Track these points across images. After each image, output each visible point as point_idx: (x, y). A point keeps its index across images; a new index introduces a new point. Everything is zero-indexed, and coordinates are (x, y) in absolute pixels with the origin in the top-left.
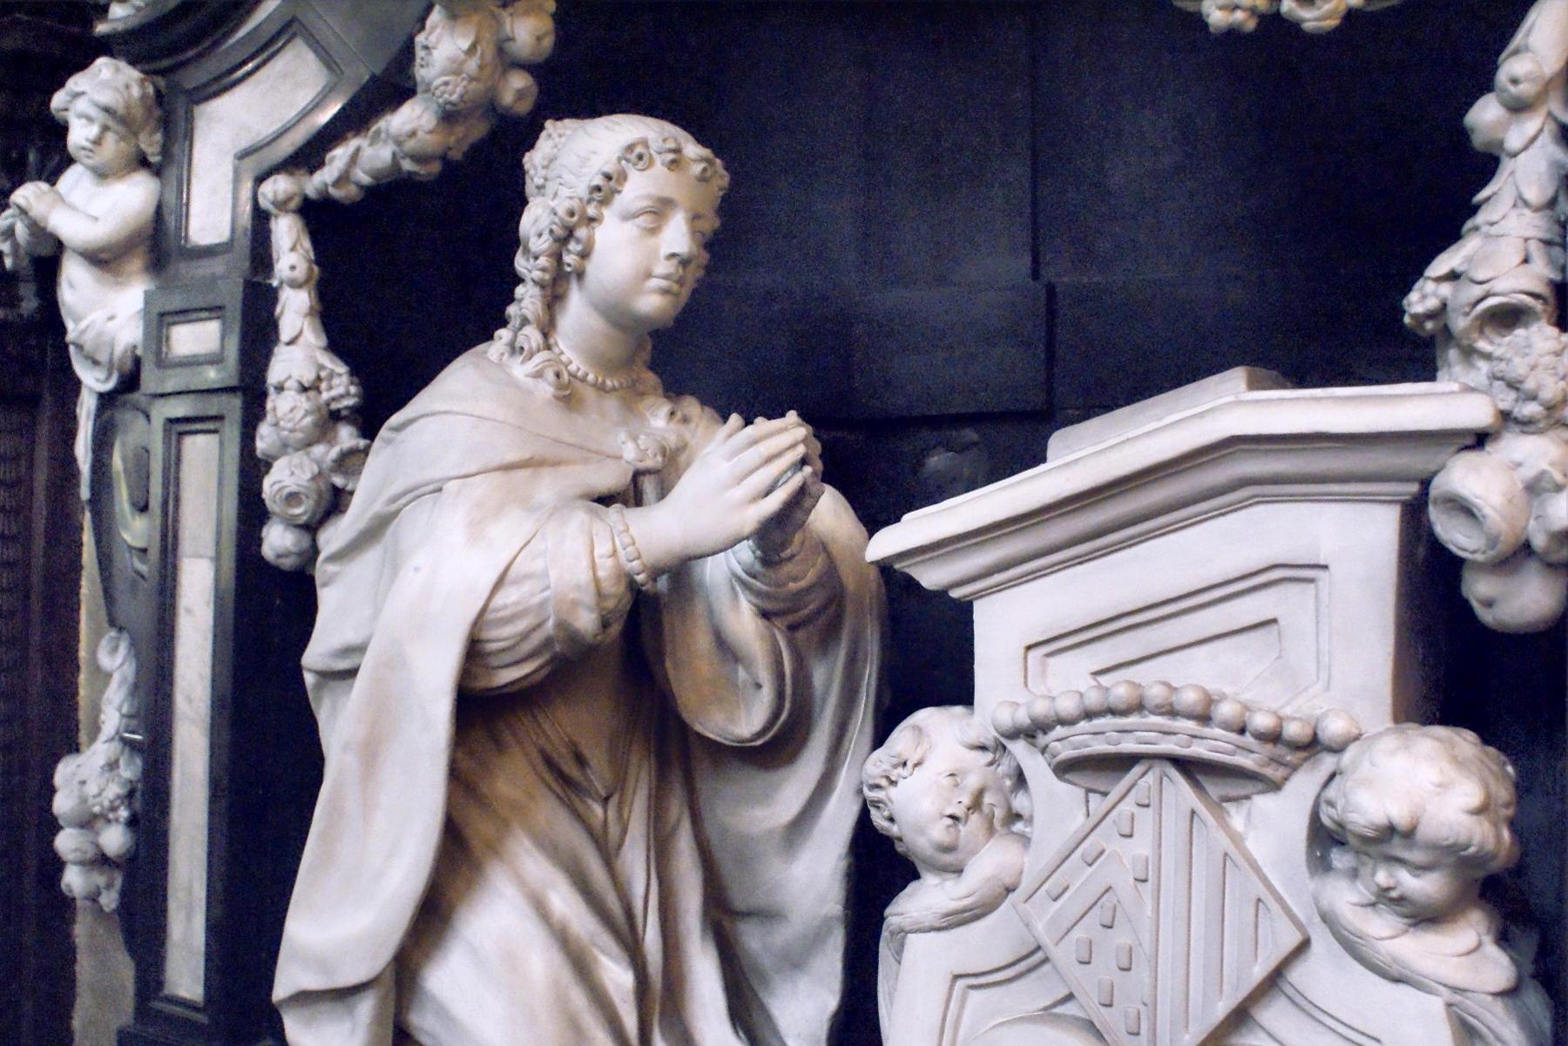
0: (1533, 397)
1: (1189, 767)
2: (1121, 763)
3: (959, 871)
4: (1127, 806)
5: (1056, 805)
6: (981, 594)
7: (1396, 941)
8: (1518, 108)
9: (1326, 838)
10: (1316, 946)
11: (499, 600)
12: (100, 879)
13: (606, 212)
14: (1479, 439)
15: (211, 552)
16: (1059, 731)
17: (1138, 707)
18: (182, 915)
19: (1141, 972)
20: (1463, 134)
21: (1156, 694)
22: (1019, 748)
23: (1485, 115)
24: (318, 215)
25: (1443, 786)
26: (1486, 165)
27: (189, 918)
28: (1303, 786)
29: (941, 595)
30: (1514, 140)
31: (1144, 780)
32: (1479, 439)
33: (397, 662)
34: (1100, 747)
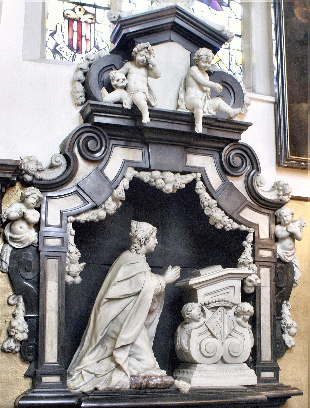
0: (255, 271)
1: (225, 307)
2: (217, 307)
3: (198, 321)
7: (98, 374)
8: (248, 243)
9: (237, 315)
18: (50, 347)
19: (220, 330)
23: (245, 243)
24: (76, 225)
28: (234, 309)
29: (195, 289)
30: (248, 246)
33: (144, 295)
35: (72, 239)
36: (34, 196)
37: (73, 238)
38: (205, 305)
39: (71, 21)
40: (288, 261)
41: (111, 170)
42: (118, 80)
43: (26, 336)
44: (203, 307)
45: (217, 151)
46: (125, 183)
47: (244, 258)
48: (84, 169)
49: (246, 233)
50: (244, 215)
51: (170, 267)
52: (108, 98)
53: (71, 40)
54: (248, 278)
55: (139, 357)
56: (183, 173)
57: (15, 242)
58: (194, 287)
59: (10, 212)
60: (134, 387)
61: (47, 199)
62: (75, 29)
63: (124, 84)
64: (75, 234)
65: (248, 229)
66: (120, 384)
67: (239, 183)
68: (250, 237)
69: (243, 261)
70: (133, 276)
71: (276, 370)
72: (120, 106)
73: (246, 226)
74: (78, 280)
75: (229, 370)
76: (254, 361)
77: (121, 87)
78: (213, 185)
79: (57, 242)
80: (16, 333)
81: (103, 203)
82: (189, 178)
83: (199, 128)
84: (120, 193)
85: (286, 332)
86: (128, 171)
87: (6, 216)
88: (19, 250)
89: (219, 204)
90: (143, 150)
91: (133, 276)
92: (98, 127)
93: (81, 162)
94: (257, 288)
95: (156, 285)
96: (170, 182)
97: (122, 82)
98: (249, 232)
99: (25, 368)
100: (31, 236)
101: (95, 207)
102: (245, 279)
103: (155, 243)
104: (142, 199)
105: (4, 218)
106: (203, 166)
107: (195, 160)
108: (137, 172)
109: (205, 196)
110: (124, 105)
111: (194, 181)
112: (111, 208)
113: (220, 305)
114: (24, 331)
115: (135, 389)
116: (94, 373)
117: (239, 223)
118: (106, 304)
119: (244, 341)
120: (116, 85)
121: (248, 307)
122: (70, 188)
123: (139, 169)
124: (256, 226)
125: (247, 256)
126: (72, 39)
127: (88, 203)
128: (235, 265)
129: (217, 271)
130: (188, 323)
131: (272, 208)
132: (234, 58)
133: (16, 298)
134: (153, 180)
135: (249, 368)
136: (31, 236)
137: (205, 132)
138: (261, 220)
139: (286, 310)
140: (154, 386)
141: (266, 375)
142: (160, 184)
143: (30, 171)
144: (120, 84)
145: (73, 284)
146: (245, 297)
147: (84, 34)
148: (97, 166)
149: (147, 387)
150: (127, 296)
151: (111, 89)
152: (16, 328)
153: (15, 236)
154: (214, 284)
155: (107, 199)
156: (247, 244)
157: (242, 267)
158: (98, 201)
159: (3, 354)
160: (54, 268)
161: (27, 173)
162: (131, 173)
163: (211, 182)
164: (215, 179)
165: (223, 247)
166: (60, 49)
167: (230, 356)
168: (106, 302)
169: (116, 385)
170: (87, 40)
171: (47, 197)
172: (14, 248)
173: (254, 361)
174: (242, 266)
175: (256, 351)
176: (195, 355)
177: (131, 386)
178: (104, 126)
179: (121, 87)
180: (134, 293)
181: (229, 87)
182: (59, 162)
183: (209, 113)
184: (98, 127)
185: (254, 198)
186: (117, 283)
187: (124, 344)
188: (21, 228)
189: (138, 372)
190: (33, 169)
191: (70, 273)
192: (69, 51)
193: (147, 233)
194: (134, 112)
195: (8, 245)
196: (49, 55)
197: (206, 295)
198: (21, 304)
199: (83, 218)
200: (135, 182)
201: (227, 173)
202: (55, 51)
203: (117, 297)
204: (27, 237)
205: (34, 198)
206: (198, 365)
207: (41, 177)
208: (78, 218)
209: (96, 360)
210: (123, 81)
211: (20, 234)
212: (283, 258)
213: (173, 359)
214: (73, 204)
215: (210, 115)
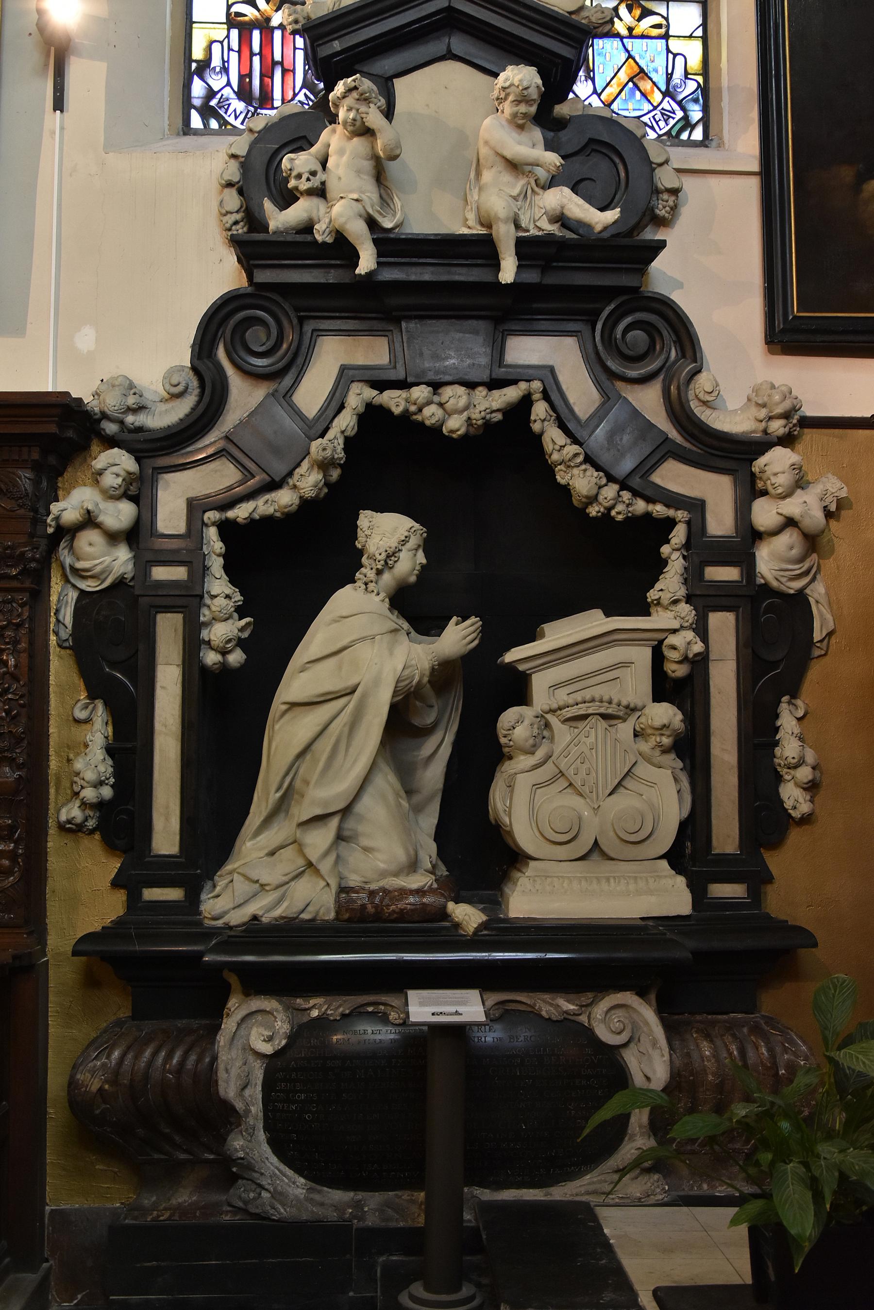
1: (605, 717)
2: (584, 717)
4: (588, 728)
5: (562, 733)
6: (534, 672)
10: (639, 762)
11: (403, 674)
12: (89, 812)
13: (403, 548)
14: (674, 631)
15: (735, 658)
16: (567, 709)
17: (593, 700)
20: (659, 553)
21: (597, 697)
22: (549, 716)
23: (665, 550)
24: (226, 529)
25: (675, 715)
26: (664, 563)
27: (167, 819)
29: (524, 672)
31: (592, 720)
32: (674, 631)
34: (582, 712)
35: (216, 565)
36: (115, 469)
37: (221, 561)
38: (552, 711)
39: (244, 28)
40: (792, 592)
41: (312, 391)
42: (299, 176)
43: (107, 792)
44: (549, 716)
45: (587, 321)
46: (346, 422)
47: (662, 590)
48: (244, 397)
49: (671, 523)
50: (663, 479)
51: (454, 619)
52: (280, 219)
53: (245, 78)
54: (666, 642)
55: (365, 842)
56: (495, 384)
57: (84, 578)
58: (521, 667)
59: (62, 511)
60: (346, 916)
61: (155, 475)
62: (256, 48)
63: (315, 182)
64: (224, 549)
65: (671, 513)
66: (310, 908)
67: (648, 401)
68: (679, 535)
69: (657, 597)
70: (345, 648)
71: (758, 879)
72: (309, 238)
73: (668, 506)
74: (236, 658)
75: (614, 878)
76: (688, 851)
77: (310, 192)
78: (576, 409)
79: (179, 573)
80: (82, 788)
81: (290, 474)
82: (511, 394)
83: (508, 273)
84: (331, 444)
85: (787, 777)
86: (351, 393)
87: (52, 521)
88: (95, 596)
89: (589, 453)
90: (391, 337)
91: (345, 648)
92: (268, 294)
93: (235, 381)
94: (700, 664)
95: (400, 667)
96: (458, 411)
97: (308, 180)
98: (677, 520)
99: (114, 865)
100: (120, 560)
101: (273, 485)
102: (661, 642)
103: (418, 562)
104: (389, 456)
105: (50, 526)
106: (551, 363)
107: (526, 350)
108: (375, 392)
109: (553, 437)
110: (317, 236)
111: (526, 402)
112: (307, 485)
113: (590, 711)
114: (101, 783)
115: (349, 920)
116: (257, 881)
117: (649, 500)
118: (287, 717)
119: (665, 799)
120: (296, 188)
121: (665, 714)
122: (212, 440)
123: (380, 385)
124: (697, 507)
125: (670, 583)
126: (250, 75)
127: (254, 477)
128: (644, 610)
129: (592, 622)
130: (510, 758)
131: (735, 455)
132: (680, 60)
133: (91, 707)
134: (413, 408)
135: (673, 872)
136: (120, 560)
137: (532, 277)
138: (716, 491)
139: (787, 721)
140: (395, 915)
141: (723, 890)
142: (431, 414)
143: (109, 413)
144: (304, 186)
145: (224, 667)
146: (663, 688)
147: (278, 57)
148: (275, 386)
149: (378, 916)
150: (333, 696)
151: (286, 199)
152: (81, 775)
153: (79, 565)
154: (583, 660)
155: (298, 465)
156: (673, 552)
157: (660, 613)
158: (279, 469)
159: (63, 833)
160: (173, 635)
161: (104, 416)
162: (359, 396)
163: (571, 401)
164: (581, 391)
165: (614, 564)
166: (221, 105)
167: (617, 841)
168: (286, 711)
169: (303, 911)
170: (285, 72)
171: (154, 469)
172: (82, 592)
173: (688, 851)
174: (659, 609)
175: (694, 828)
176: (524, 836)
177: (337, 913)
178: (287, 285)
179: (310, 192)
180: (346, 689)
181: (600, 153)
182: (178, 385)
183: (540, 229)
184: (268, 294)
185: (690, 435)
186: (308, 665)
187: (319, 811)
188: (90, 543)
189: (364, 880)
190: (116, 408)
191: (212, 643)
192: (239, 106)
193: (392, 543)
194: (342, 249)
195: (69, 586)
196: (196, 121)
197: (555, 687)
198: (100, 719)
199: (241, 512)
200: (372, 415)
201: (614, 376)
202: (207, 112)
203: (306, 700)
204: (106, 564)
205: (118, 475)
206: (532, 864)
207: (137, 424)
208: (231, 514)
209: (266, 851)
210: (311, 177)
211: (89, 560)
212: (775, 584)
213: (477, 852)
214: (220, 477)
215: (540, 233)
